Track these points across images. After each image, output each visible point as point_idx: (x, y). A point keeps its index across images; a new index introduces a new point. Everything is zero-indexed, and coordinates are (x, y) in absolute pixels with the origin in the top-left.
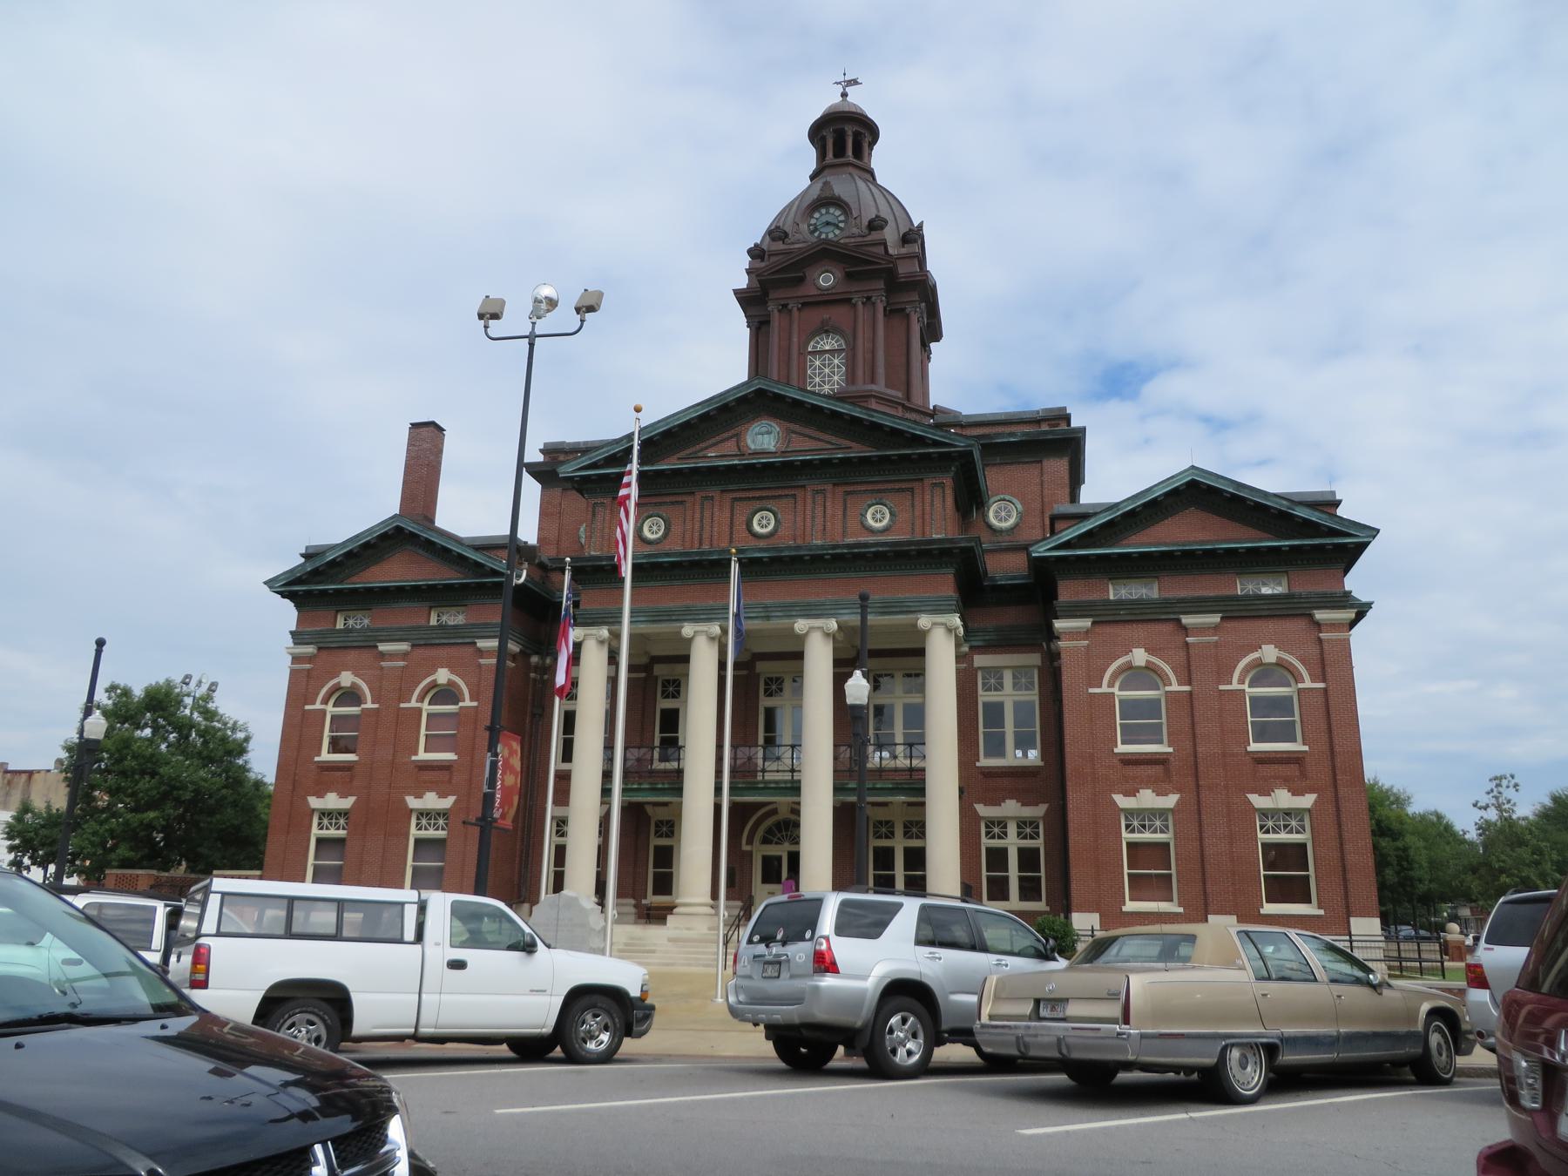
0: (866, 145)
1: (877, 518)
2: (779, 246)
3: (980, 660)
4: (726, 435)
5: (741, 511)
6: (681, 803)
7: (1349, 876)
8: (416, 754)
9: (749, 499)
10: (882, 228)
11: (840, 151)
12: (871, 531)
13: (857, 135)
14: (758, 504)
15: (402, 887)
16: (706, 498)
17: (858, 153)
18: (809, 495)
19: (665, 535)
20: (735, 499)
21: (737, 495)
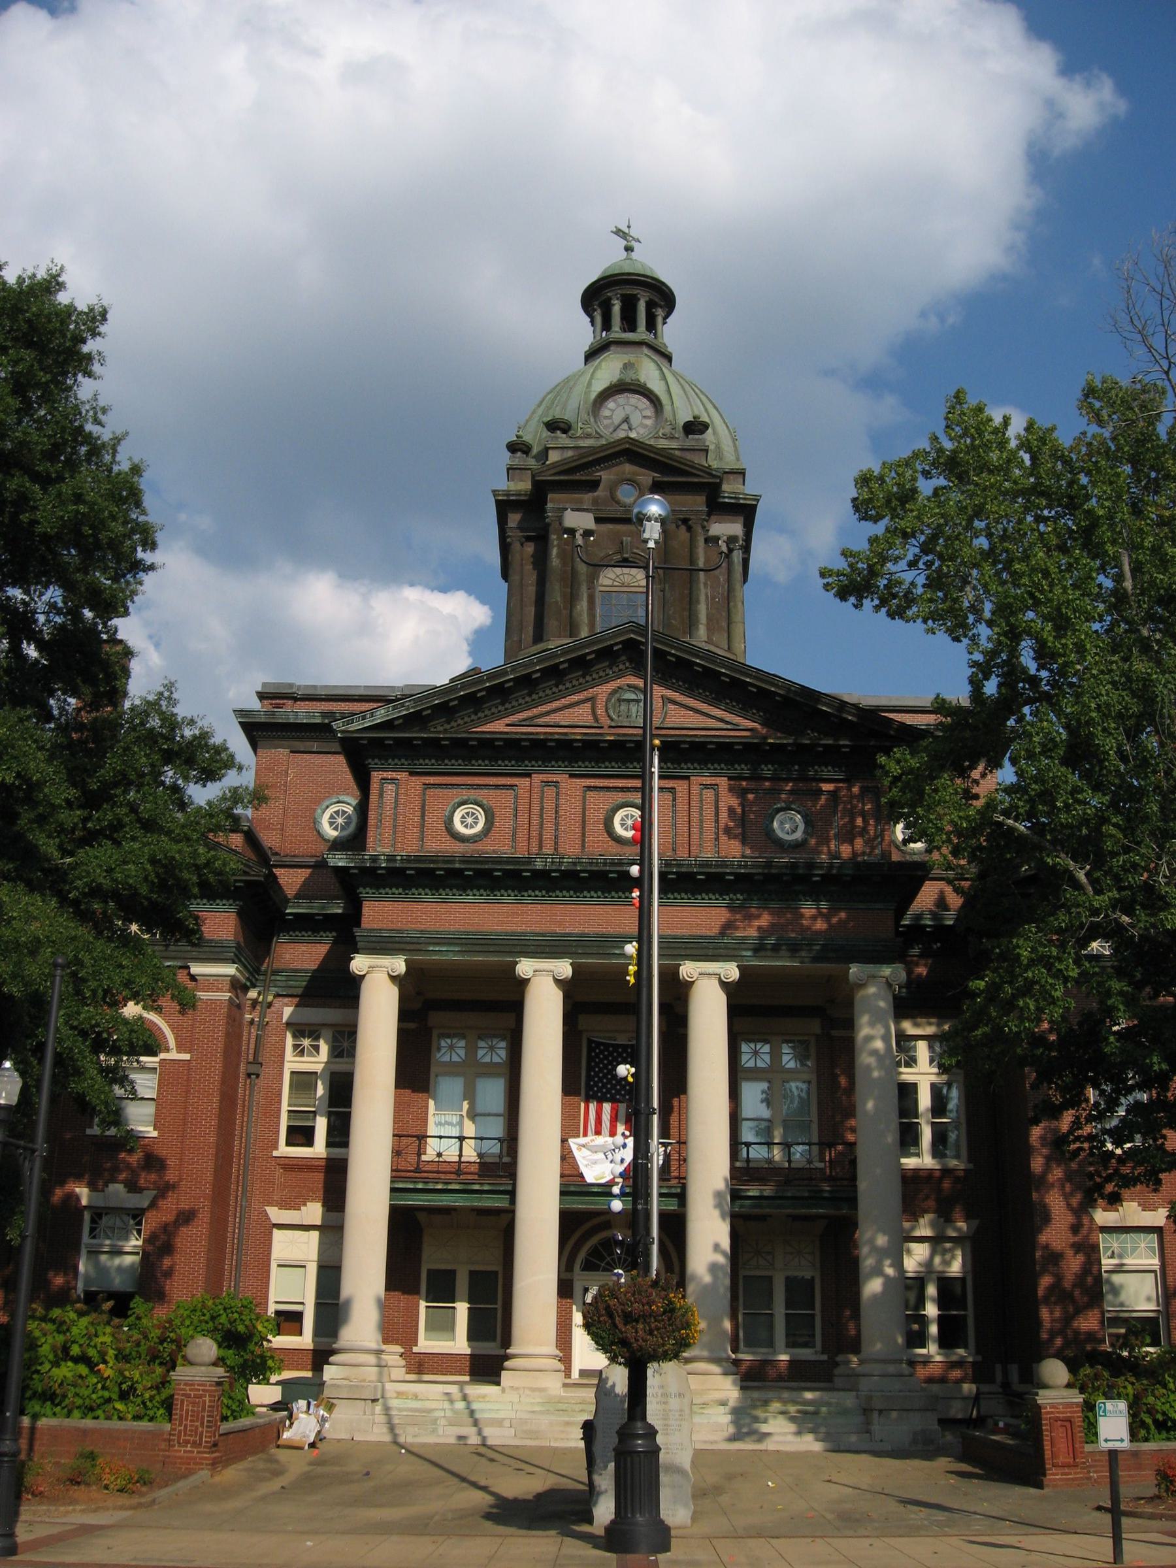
0: (660, 319)
1: (468, 821)
2: (562, 439)
3: (634, 1042)
4: (575, 698)
5: (439, 800)
6: (856, 1214)
7: (473, 1478)
8: (276, 1148)
9: (608, 788)
10: (702, 432)
11: (630, 323)
12: (462, 839)
13: (650, 305)
14: (465, 794)
15: (787, 1308)
16: (547, 783)
17: (651, 326)
18: (695, 789)
19: (487, 831)
20: (428, 786)
21: (432, 780)
